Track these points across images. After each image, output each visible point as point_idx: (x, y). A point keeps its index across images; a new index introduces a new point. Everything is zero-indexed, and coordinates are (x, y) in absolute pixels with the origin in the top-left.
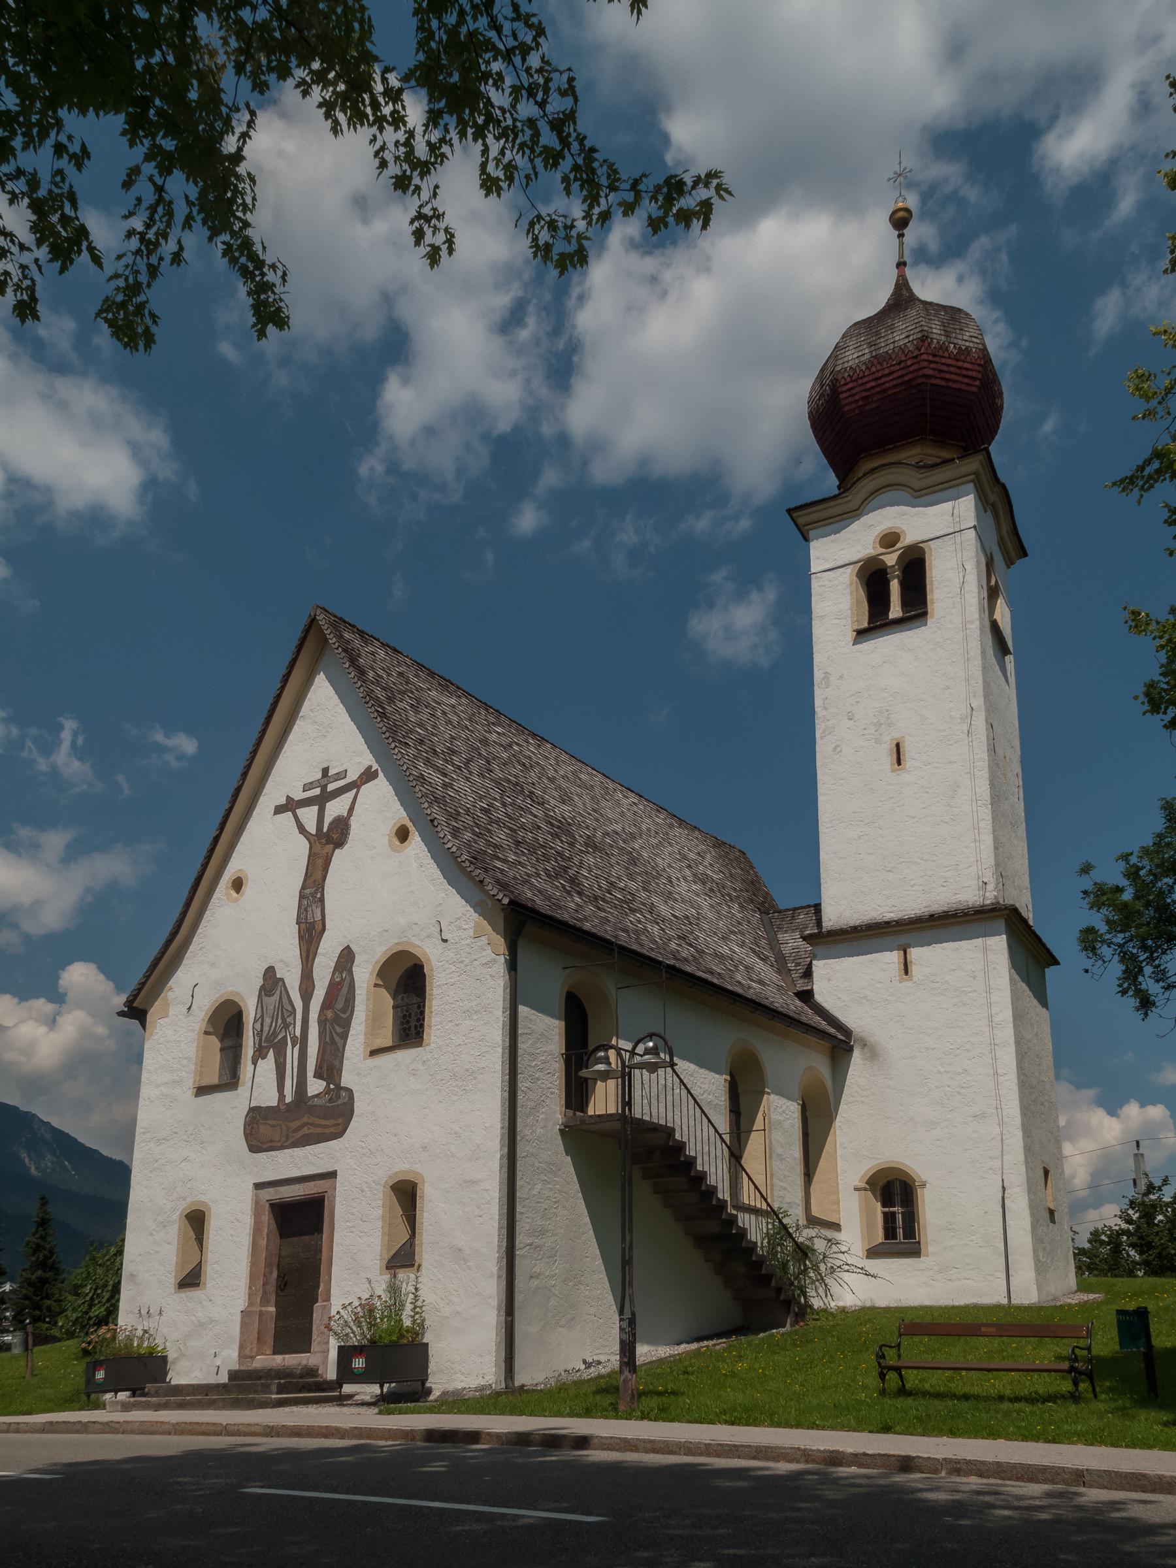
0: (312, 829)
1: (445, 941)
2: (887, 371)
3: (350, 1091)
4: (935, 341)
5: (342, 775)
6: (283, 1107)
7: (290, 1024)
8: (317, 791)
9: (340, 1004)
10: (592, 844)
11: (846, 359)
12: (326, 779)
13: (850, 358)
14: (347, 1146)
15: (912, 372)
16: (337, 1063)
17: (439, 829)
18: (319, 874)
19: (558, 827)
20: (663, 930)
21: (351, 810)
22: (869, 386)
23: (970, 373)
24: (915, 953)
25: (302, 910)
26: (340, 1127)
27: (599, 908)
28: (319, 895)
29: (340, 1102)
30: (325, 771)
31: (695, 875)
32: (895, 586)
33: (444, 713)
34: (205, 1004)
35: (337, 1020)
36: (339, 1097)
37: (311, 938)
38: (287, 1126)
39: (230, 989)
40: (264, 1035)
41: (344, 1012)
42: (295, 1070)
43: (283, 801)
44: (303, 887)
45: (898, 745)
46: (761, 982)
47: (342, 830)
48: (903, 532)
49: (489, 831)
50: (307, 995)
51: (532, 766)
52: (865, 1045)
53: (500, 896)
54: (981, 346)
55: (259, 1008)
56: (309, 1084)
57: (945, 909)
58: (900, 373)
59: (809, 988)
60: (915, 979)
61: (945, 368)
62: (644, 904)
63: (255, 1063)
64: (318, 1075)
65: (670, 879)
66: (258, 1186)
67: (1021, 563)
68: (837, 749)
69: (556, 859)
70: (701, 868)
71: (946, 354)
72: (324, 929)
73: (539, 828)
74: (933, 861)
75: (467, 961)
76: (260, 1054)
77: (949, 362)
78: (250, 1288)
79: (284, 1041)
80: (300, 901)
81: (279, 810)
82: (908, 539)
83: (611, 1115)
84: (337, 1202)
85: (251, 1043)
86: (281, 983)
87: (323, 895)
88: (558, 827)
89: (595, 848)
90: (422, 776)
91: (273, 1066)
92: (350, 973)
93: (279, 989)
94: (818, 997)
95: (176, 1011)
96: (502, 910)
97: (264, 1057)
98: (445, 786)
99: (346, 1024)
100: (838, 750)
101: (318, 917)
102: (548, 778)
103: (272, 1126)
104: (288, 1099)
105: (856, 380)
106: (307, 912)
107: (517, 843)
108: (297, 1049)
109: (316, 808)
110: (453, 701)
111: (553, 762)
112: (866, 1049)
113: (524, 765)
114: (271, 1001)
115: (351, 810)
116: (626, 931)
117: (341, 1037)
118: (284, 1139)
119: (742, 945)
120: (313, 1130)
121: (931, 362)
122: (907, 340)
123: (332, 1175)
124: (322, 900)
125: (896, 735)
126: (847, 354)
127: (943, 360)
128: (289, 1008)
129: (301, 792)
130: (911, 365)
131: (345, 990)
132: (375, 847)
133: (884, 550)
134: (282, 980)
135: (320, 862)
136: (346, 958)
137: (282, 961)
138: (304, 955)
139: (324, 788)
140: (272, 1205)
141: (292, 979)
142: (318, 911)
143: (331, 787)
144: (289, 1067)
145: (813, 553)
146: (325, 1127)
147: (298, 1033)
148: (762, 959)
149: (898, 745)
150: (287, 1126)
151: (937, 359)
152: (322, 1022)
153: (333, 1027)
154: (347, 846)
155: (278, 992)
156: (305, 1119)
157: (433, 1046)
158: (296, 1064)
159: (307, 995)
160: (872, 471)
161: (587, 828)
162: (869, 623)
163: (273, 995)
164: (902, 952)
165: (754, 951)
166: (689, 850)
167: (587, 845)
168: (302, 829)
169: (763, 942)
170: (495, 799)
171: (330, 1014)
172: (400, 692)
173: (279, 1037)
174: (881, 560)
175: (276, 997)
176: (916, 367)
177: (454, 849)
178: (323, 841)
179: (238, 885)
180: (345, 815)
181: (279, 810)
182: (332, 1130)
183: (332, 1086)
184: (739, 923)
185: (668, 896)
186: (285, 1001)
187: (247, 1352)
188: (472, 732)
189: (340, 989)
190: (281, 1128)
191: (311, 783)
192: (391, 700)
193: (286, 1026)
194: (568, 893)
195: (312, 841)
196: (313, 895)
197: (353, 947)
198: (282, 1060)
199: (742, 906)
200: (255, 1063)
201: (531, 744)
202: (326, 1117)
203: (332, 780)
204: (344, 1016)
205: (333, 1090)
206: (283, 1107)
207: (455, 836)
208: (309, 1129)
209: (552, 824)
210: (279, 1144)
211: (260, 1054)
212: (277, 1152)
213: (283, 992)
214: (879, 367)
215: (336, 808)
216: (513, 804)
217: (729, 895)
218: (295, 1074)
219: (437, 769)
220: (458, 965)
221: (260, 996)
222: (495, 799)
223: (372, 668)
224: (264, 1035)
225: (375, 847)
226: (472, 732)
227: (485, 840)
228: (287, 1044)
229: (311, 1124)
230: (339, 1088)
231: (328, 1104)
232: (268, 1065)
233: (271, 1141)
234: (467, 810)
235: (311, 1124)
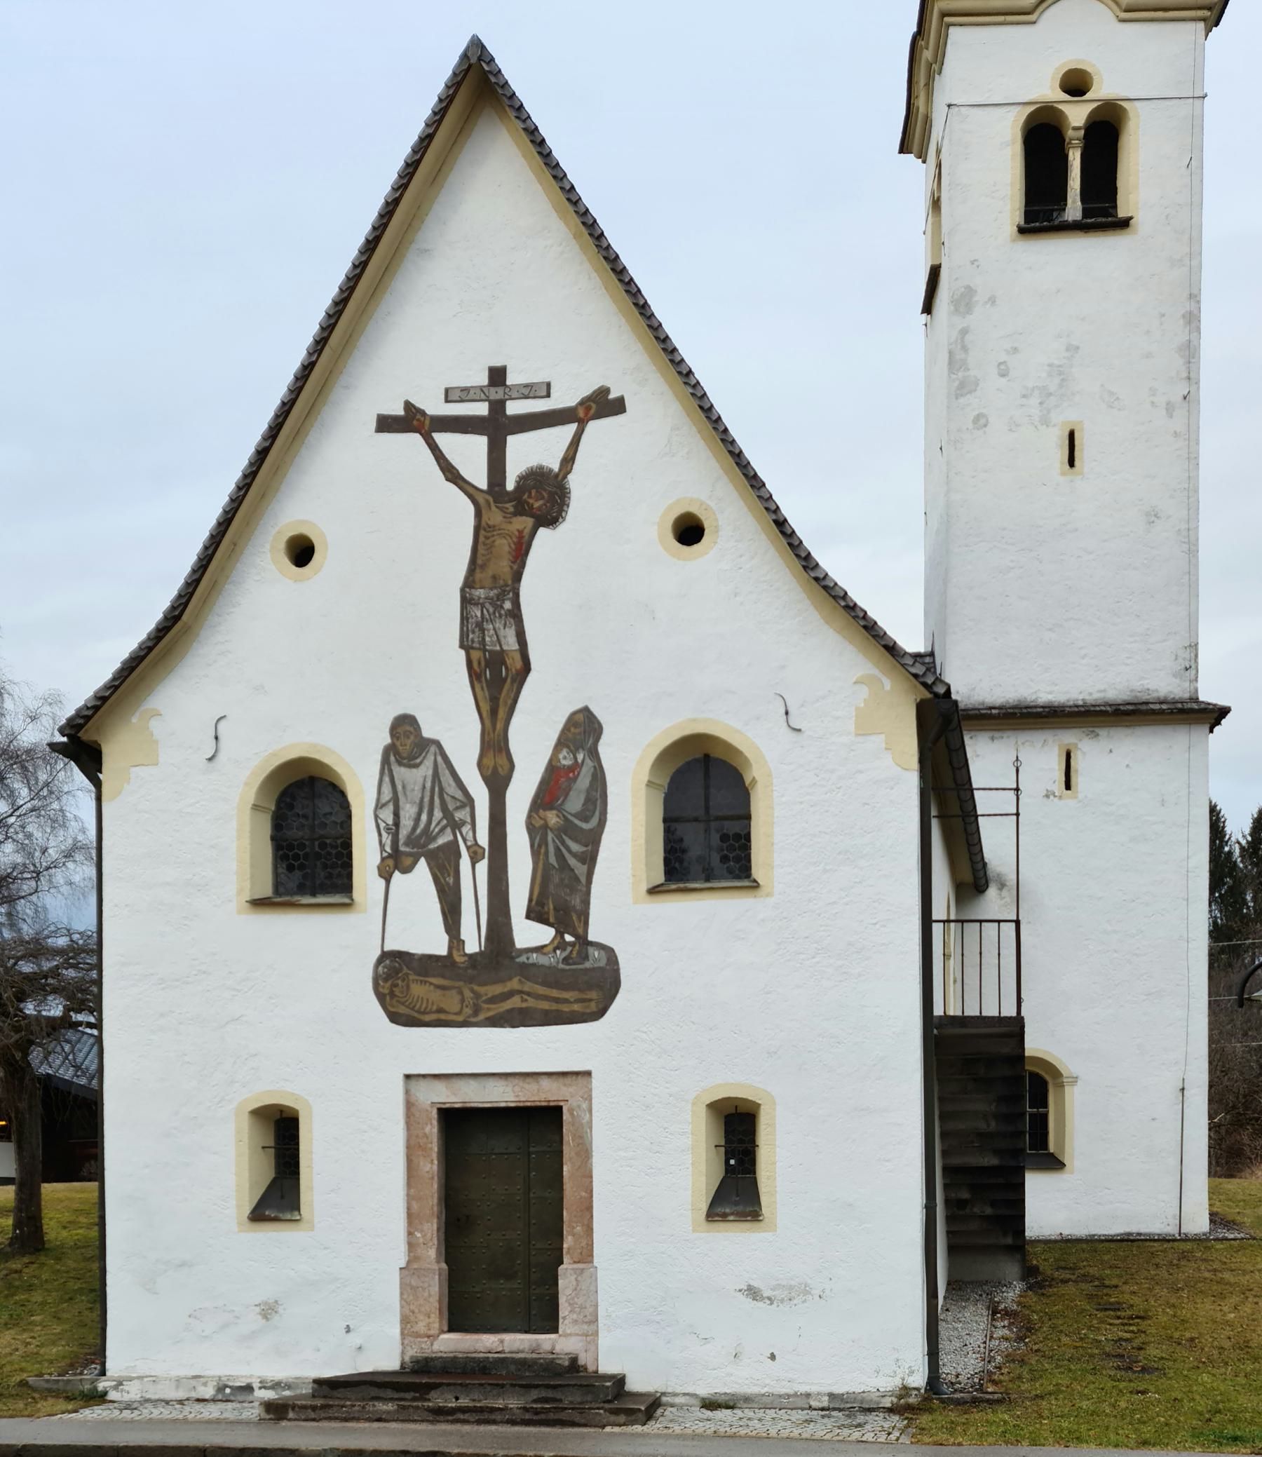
0: (480, 479)
3: (610, 953)
6: (458, 958)
7: (463, 823)
9: (575, 803)
16: (576, 901)
18: (503, 566)
21: (569, 459)
26: (593, 1004)
35: (567, 829)
38: (472, 991)
44: (469, 583)
45: (1072, 435)
60: (1081, 796)
64: (536, 913)
72: (526, 668)
78: (410, 1234)
79: (452, 851)
82: (1102, 90)
86: (433, 749)
92: (594, 754)
97: (407, 870)
100: (982, 421)
101: (511, 643)
103: (438, 987)
106: (483, 630)
108: (483, 867)
114: (415, 778)
115: (569, 459)
117: (583, 861)
118: (468, 1011)
120: (531, 1003)
128: (459, 795)
131: (584, 781)
135: (504, 546)
138: (486, 707)
140: (440, 1110)
147: (483, 839)
149: (1072, 435)
152: (536, 830)
153: (563, 843)
156: (514, 984)
159: (498, 782)
163: (417, 766)
171: (552, 818)
175: (426, 770)
179: (302, 552)
180: (556, 467)
182: (576, 1007)
183: (568, 938)
187: (421, 1327)
189: (576, 778)
190: (461, 993)
198: (451, 880)
200: (386, 875)
202: (557, 985)
203: (514, 395)
208: (523, 1000)
210: (460, 1018)
221: (385, 762)
228: (459, 855)
229: (529, 994)
231: (561, 966)
235: (529, 994)
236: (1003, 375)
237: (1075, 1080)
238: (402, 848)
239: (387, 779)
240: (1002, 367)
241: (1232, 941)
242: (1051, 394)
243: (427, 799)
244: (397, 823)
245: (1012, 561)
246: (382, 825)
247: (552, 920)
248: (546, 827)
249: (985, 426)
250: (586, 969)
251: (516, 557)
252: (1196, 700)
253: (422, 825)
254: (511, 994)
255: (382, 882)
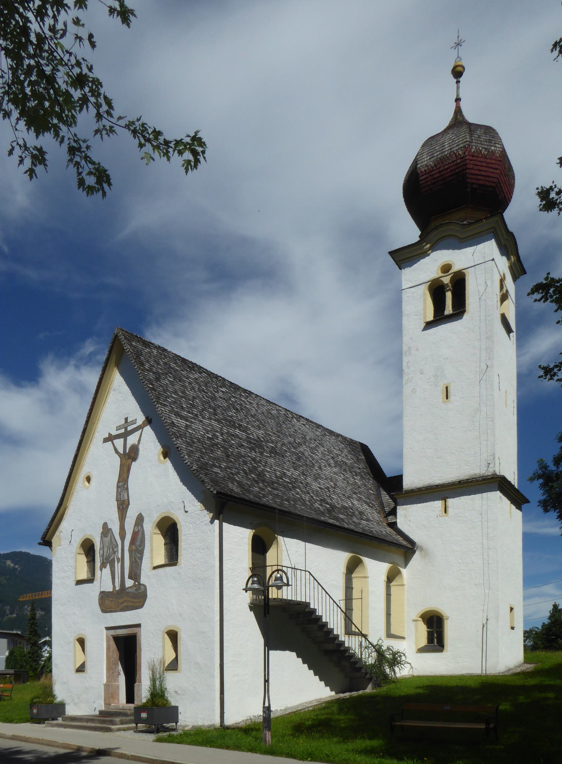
1: (186, 512)
2: (446, 167)
3: (145, 586)
4: (474, 147)
5: (134, 422)
6: (115, 592)
8: (123, 431)
10: (273, 451)
11: (423, 160)
12: (127, 424)
13: (425, 159)
14: (145, 612)
15: (461, 167)
16: (138, 572)
17: (181, 452)
19: (254, 444)
20: (312, 497)
21: (139, 441)
22: (435, 176)
23: (494, 166)
24: (450, 501)
25: (118, 494)
27: (274, 489)
28: (126, 486)
29: (140, 591)
30: (126, 419)
31: (336, 462)
32: (449, 295)
33: (190, 383)
34: (78, 540)
36: (140, 589)
37: (123, 508)
38: (117, 601)
39: (88, 533)
40: (105, 556)
41: (140, 547)
42: (120, 574)
43: (107, 436)
44: (118, 482)
45: (447, 388)
46: (368, 520)
47: (136, 451)
48: (453, 263)
49: (212, 451)
50: (123, 537)
51: (242, 409)
52: (422, 550)
53: (212, 490)
54: (501, 149)
55: (102, 543)
56: (126, 581)
57: (467, 478)
58: (454, 168)
59: (395, 521)
60: (449, 515)
61: (480, 164)
62: (302, 483)
63: (101, 570)
64: (130, 577)
65: (320, 468)
66: (108, 629)
67: (523, 277)
68: (414, 391)
69: (251, 463)
70: (340, 457)
71: (480, 155)
73: (243, 445)
74: (463, 452)
75: (198, 522)
76: (103, 566)
77: (482, 160)
80: (117, 489)
81: (106, 440)
82: (455, 269)
83: (274, 599)
84: (142, 638)
85: (99, 560)
86: (110, 531)
87: (127, 486)
88: (254, 444)
89: (276, 453)
90: (173, 423)
91: (109, 572)
92: (142, 527)
93: (110, 534)
94: (399, 526)
95: (65, 542)
96: (213, 496)
97: (105, 567)
98: (187, 427)
99: (142, 553)
101: (126, 498)
102: (252, 415)
104: (117, 588)
105: (428, 173)
106: (121, 495)
107: (228, 456)
108: (120, 564)
109: (122, 440)
110: (196, 376)
111: (255, 405)
112: (423, 552)
113: (237, 409)
114: (107, 540)
115: (139, 441)
116: (287, 500)
119: (359, 499)
121: (471, 160)
122: (457, 148)
123: (139, 626)
124: (127, 489)
125: (446, 382)
126: (424, 157)
127: (479, 159)
129: (115, 431)
130: (460, 163)
132: (151, 461)
133: (443, 275)
134: (111, 529)
136: (140, 519)
137: (110, 520)
139: (126, 428)
141: (115, 528)
142: (126, 494)
143: (129, 428)
144: (116, 572)
145: (404, 277)
146: (134, 602)
147: (120, 556)
148: (369, 506)
149: (447, 388)
150: (117, 601)
151: (475, 158)
152: (130, 551)
154: (138, 460)
155: (109, 536)
156: (125, 598)
157: (182, 565)
158: (120, 571)
159: (123, 537)
160: (436, 228)
161: (272, 442)
162: (434, 317)
163: (107, 537)
164: (444, 501)
165: (366, 503)
166: (334, 448)
167: (271, 452)
168: (116, 451)
169: (372, 497)
170: (217, 432)
171: (134, 548)
172: (163, 374)
173: (112, 558)
174: (441, 280)
175: (109, 538)
176: (462, 163)
177: (189, 464)
178: (127, 457)
179: (88, 479)
180: (137, 443)
181: (106, 440)
182: (138, 604)
183: (137, 583)
184: (359, 487)
185: (317, 478)
186: (113, 539)
188: (206, 393)
189: (138, 535)
191: (120, 426)
192: (158, 379)
193: (114, 553)
194: (256, 481)
195: (122, 457)
196: (123, 486)
197: (143, 514)
199: (362, 477)
200: (101, 570)
201: (243, 396)
203: (129, 424)
204: (140, 549)
205: (137, 585)
206: (115, 592)
207: (189, 456)
209: (250, 442)
211: (103, 566)
212: (114, 613)
213: (112, 536)
214: (441, 165)
215: (132, 440)
216: (228, 433)
217: (355, 472)
218: (120, 576)
219: (182, 417)
220: (194, 524)
221: (101, 537)
222: (217, 432)
223: (148, 361)
224: (105, 556)
225: (151, 461)
226: (206, 393)
227: (209, 456)
228: (115, 562)
229: (128, 601)
230: (140, 584)
231: (135, 592)
232: (107, 571)
233: (111, 608)
234: (199, 440)
236: (421, 374)
237: (447, 619)
238: (105, 561)
239: (102, 541)
240: (421, 371)
241: (174, 561)
242: (438, 376)
243: (109, 546)
244: (103, 554)
245: (425, 436)
246: (101, 555)
247: (133, 578)
248: (132, 550)
249: (416, 392)
250: (140, 592)
251: (128, 472)
252: (496, 474)
253: (108, 554)
254: (124, 602)
255: (100, 572)
